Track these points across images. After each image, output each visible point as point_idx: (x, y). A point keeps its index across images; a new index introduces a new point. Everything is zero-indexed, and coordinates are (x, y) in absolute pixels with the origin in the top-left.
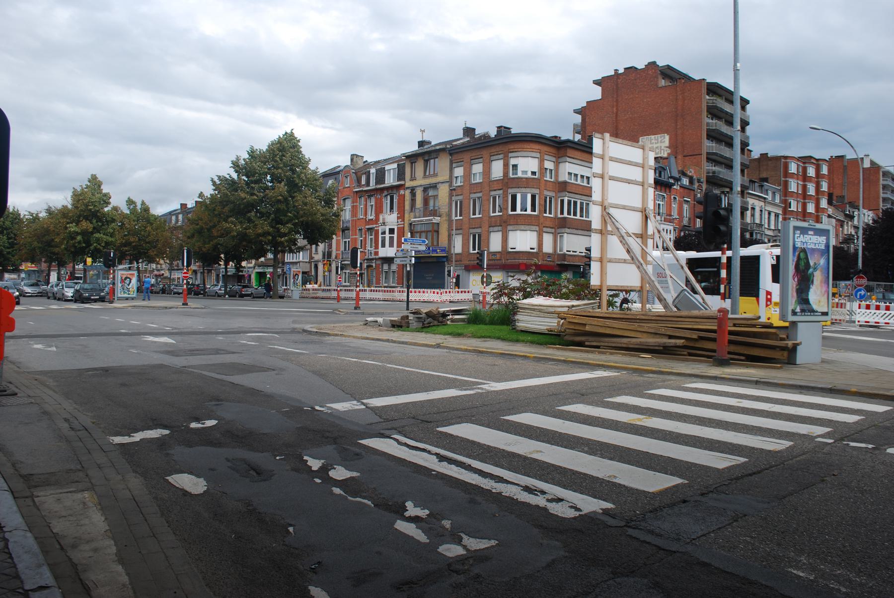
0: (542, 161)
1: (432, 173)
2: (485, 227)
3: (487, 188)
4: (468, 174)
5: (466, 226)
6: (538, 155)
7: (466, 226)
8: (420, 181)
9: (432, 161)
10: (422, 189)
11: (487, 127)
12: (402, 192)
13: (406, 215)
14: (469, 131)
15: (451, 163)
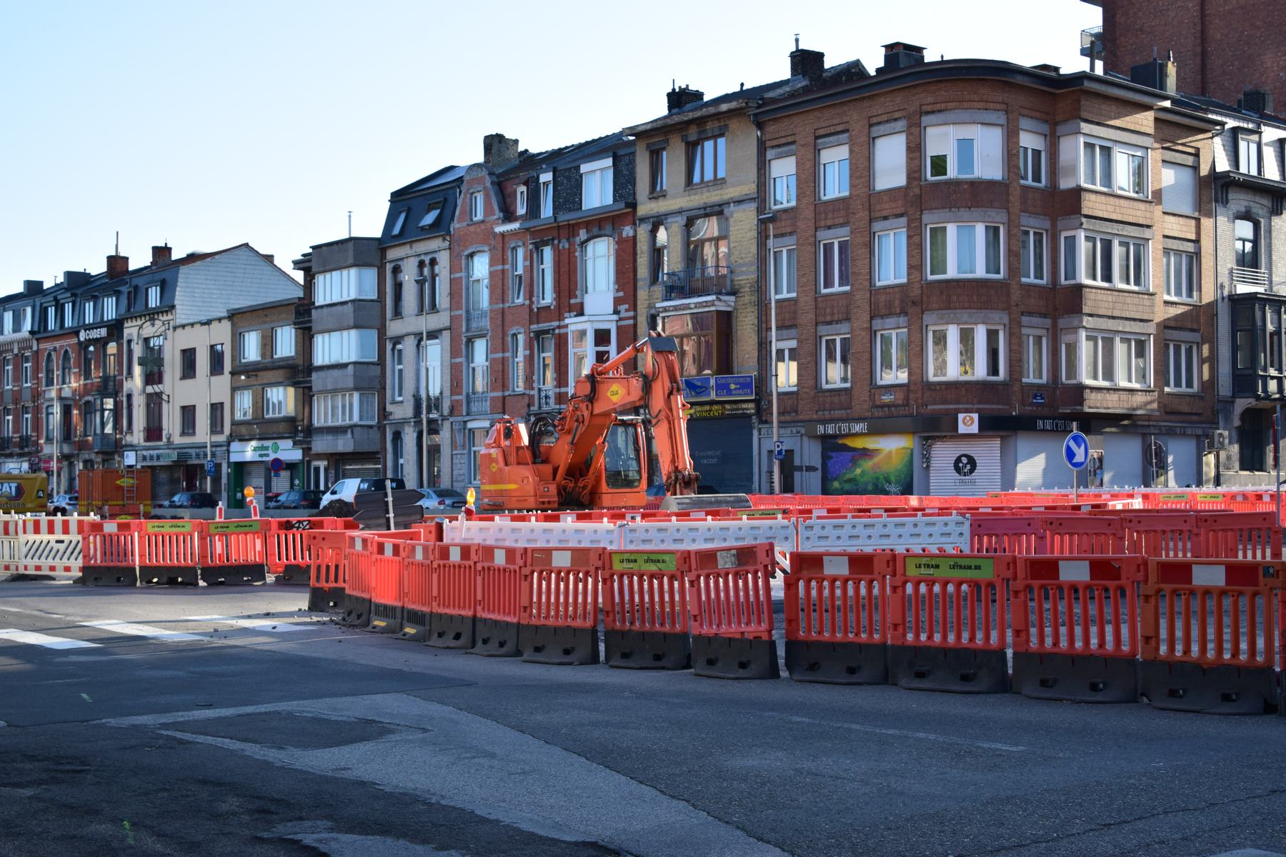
0: (1011, 136)
1: (709, 176)
2: (862, 317)
3: (863, 215)
4: (809, 178)
5: (807, 318)
6: (1002, 118)
7: (807, 318)
8: (678, 200)
9: (709, 145)
10: (681, 220)
11: (856, 45)
12: (628, 231)
13: (642, 294)
14: (805, 61)
15: (762, 148)
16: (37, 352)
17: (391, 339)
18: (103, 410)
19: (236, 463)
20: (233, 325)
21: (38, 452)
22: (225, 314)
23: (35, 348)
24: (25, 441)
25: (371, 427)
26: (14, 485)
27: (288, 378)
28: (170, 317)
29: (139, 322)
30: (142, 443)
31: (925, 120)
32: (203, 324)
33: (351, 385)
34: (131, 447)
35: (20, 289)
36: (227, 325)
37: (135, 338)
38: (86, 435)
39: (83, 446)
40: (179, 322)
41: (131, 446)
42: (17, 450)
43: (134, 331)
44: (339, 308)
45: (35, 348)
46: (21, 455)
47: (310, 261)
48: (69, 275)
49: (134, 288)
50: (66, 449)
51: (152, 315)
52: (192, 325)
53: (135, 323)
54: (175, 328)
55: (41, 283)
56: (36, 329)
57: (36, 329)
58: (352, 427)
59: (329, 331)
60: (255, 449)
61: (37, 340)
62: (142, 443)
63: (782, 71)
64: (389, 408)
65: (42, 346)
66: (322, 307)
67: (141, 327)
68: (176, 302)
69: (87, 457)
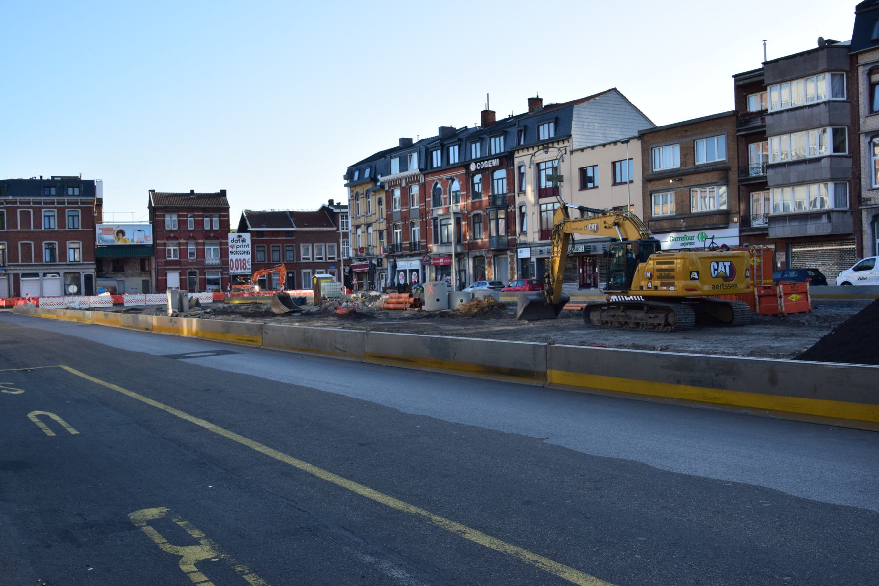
14: (535, 102)
16: (424, 184)
17: (867, 134)
18: (497, 220)
19: (522, 259)
20: (642, 143)
21: (427, 252)
22: (637, 134)
23: (422, 181)
24: (413, 246)
25: (845, 212)
26: (727, 264)
27: (722, 179)
28: (566, 144)
29: (531, 151)
30: (537, 240)
31: (146, 238)
32: (622, 142)
33: (828, 176)
34: (525, 245)
35: (397, 144)
36: (636, 145)
37: (527, 163)
38: (475, 239)
39: (472, 246)
40: (575, 147)
41: (526, 244)
42: (408, 252)
43: (527, 160)
44: (806, 110)
45: (422, 181)
46: (412, 256)
47: (762, 75)
48: (442, 129)
49: (548, 120)
50: (459, 250)
51: (546, 145)
52: (593, 148)
53: (526, 152)
54: (572, 152)
55: (411, 140)
56: (423, 167)
57: (423, 167)
58: (828, 213)
59: (790, 132)
60: (675, 240)
61: (425, 175)
62: (537, 240)
63: (524, 109)
64: (865, 194)
65: (429, 179)
66: (772, 114)
67: (533, 155)
68: (573, 133)
69: (474, 254)
